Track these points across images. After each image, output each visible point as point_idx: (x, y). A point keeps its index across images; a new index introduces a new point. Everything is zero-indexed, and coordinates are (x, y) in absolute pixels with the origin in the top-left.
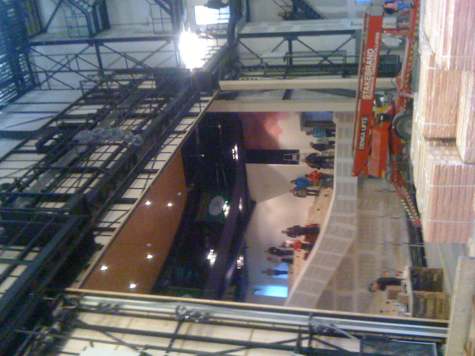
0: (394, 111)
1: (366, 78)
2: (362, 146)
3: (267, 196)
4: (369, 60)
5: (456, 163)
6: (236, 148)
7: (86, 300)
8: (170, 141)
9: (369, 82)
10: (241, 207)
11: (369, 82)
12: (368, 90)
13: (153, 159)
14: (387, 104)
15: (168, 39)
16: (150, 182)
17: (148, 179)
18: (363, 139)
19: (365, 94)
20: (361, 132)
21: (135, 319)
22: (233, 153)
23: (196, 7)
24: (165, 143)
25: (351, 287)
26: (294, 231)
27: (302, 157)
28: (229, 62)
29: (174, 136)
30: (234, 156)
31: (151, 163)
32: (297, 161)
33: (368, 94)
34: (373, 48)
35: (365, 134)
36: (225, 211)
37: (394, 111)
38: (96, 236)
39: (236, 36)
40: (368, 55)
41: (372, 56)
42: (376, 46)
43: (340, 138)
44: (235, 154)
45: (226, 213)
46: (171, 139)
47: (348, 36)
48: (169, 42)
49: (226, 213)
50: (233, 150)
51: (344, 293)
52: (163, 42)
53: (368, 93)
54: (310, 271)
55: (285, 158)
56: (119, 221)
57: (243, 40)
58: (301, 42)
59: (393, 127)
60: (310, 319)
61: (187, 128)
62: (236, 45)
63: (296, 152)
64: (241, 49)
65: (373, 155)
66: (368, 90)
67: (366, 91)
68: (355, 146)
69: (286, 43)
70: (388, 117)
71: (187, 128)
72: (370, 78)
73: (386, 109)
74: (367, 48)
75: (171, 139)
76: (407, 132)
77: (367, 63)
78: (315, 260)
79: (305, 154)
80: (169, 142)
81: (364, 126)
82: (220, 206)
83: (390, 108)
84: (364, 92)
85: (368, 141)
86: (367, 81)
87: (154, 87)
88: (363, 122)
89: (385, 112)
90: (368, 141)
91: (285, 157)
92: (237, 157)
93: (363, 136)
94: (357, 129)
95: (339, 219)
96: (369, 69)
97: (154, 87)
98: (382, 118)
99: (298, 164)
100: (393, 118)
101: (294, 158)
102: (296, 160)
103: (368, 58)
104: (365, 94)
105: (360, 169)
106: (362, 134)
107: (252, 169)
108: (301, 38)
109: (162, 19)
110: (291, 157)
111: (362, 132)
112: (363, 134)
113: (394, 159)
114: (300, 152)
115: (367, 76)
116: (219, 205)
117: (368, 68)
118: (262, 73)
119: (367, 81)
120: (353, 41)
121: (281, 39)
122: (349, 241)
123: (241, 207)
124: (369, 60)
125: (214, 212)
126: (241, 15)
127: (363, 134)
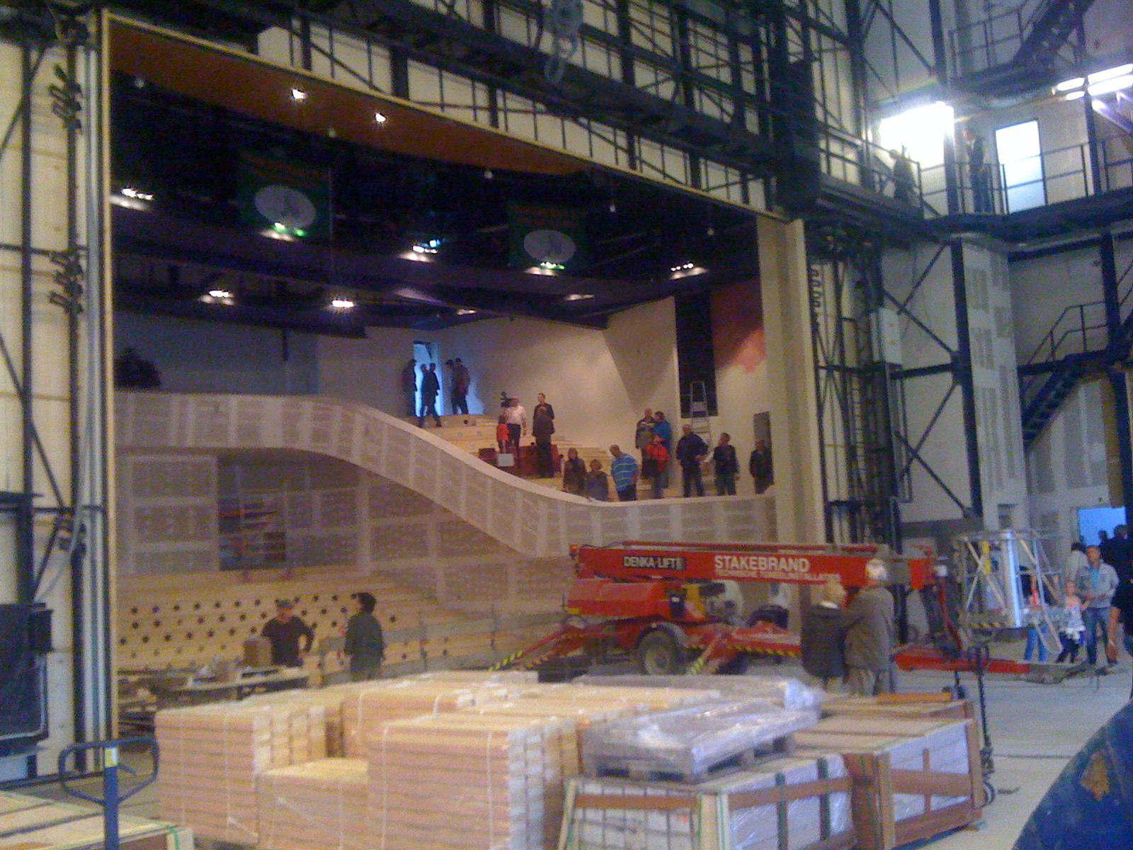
0: (690, 625)
1: (754, 560)
2: (631, 561)
3: (619, 350)
4: (787, 561)
5: (262, 757)
6: (697, 271)
7: (88, 54)
8: (604, 134)
9: (746, 566)
10: (574, 297)
11: (746, 566)
12: (733, 565)
13: (540, 106)
14: (708, 608)
15: (938, 68)
16: (465, 117)
17: (475, 108)
18: (643, 562)
19: (723, 561)
20: (656, 556)
21: (64, 163)
22: (685, 267)
23: (1034, 124)
24: (594, 125)
25: (446, 553)
26: (544, 419)
27: (697, 424)
28: (875, 231)
29: (622, 141)
30: (679, 268)
31: (525, 104)
32: (691, 414)
33: (724, 568)
34: (811, 571)
35: (651, 567)
36: (542, 268)
37: (690, 625)
38: (289, 28)
39: (954, 236)
40: (796, 560)
41: (796, 569)
42: (815, 575)
43: (686, 508)
44: (683, 270)
45: (536, 271)
46: (611, 137)
47: (967, 502)
48: (931, 71)
49: (536, 271)
50: (691, 266)
51: (432, 539)
52: (931, 60)
53: (727, 566)
54: (453, 464)
55: (694, 385)
56: (338, 69)
57: (947, 253)
58: (949, 394)
59: (654, 625)
60: (92, 508)
61: (653, 168)
62: (934, 240)
63: (712, 409)
64: (927, 253)
65: (610, 586)
66: (733, 565)
67: (730, 560)
68: (629, 548)
69: (946, 359)
70: (678, 613)
71: (653, 168)
72: (755, 568)
73: (695, 608)
74: (809, 558)
75: (611, 137)
76: (647, 655)
77: (783, 560)
78: (475, 473)
79: (707, 430)
80: (598, 132)
81: (666, 562)
82: (548, 253)
83: (698, 615)
84: (727, 558)
85: (642, 575)
86: (748, 562)
87: (792, 59)
88: (673, 560)
89: (689, 605)
90: (642, 575)
91: (699, 385)
92: (677, 276)
93: (648, 561)
94: (660, 548)
95: (553, 517)
96: (771, 564)
97: (792, 59)
98: (675, 600)
99: (682, 417)
100: (677, 623)
101: (699, 406)
102: (692, 410)
103: (791, 560)
104: (723, 561)
105: (593, 561)
106: (652, 559)
107: (665, 311)
108: (959, 389)
109: (993, 43)
110: (698, 398)
111: (655, 560)
112: (651, 563)
113: (604, 632)
114: (712, 418)
115: (757, 561)
116: (550, 254)
117: (773, 562)
118: (846, 313)
119: (748, 562)
120: (957, 514)
121: (954, 346)
122: (517, 543)
123: (574, 297)
124: (787, 561)
125: (532, 242)
126: (1015, 239)
127: (651, 563)
